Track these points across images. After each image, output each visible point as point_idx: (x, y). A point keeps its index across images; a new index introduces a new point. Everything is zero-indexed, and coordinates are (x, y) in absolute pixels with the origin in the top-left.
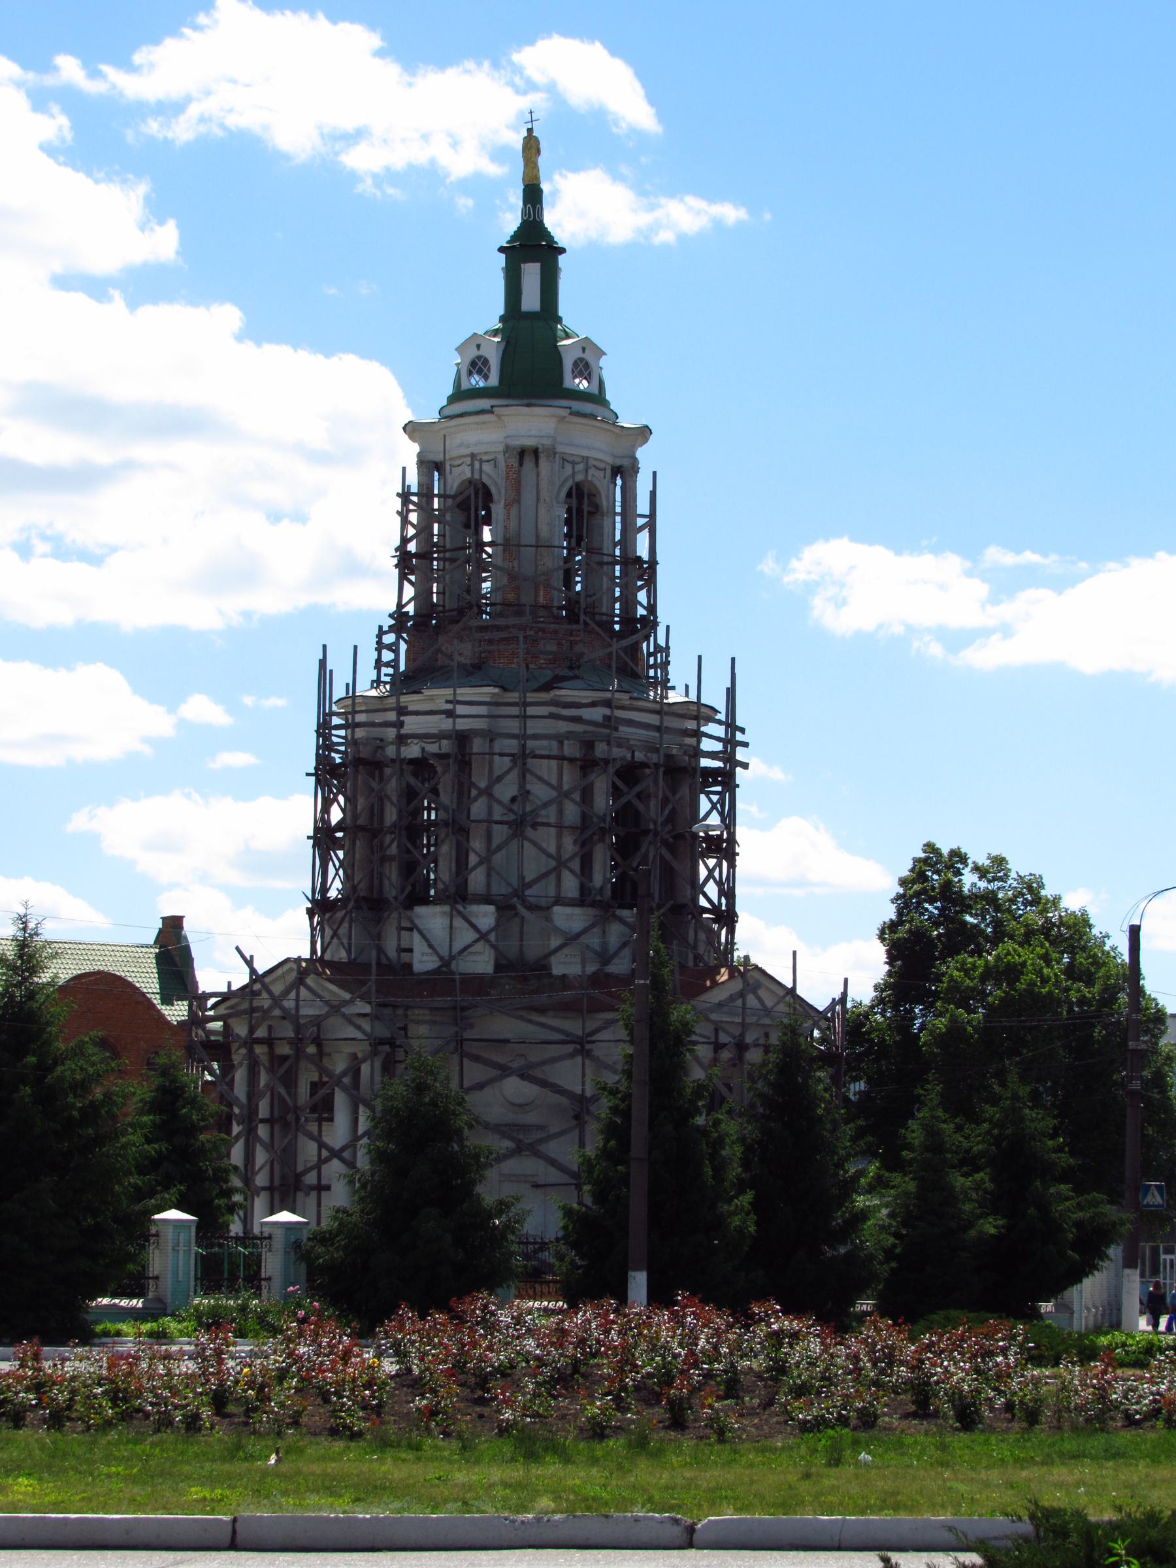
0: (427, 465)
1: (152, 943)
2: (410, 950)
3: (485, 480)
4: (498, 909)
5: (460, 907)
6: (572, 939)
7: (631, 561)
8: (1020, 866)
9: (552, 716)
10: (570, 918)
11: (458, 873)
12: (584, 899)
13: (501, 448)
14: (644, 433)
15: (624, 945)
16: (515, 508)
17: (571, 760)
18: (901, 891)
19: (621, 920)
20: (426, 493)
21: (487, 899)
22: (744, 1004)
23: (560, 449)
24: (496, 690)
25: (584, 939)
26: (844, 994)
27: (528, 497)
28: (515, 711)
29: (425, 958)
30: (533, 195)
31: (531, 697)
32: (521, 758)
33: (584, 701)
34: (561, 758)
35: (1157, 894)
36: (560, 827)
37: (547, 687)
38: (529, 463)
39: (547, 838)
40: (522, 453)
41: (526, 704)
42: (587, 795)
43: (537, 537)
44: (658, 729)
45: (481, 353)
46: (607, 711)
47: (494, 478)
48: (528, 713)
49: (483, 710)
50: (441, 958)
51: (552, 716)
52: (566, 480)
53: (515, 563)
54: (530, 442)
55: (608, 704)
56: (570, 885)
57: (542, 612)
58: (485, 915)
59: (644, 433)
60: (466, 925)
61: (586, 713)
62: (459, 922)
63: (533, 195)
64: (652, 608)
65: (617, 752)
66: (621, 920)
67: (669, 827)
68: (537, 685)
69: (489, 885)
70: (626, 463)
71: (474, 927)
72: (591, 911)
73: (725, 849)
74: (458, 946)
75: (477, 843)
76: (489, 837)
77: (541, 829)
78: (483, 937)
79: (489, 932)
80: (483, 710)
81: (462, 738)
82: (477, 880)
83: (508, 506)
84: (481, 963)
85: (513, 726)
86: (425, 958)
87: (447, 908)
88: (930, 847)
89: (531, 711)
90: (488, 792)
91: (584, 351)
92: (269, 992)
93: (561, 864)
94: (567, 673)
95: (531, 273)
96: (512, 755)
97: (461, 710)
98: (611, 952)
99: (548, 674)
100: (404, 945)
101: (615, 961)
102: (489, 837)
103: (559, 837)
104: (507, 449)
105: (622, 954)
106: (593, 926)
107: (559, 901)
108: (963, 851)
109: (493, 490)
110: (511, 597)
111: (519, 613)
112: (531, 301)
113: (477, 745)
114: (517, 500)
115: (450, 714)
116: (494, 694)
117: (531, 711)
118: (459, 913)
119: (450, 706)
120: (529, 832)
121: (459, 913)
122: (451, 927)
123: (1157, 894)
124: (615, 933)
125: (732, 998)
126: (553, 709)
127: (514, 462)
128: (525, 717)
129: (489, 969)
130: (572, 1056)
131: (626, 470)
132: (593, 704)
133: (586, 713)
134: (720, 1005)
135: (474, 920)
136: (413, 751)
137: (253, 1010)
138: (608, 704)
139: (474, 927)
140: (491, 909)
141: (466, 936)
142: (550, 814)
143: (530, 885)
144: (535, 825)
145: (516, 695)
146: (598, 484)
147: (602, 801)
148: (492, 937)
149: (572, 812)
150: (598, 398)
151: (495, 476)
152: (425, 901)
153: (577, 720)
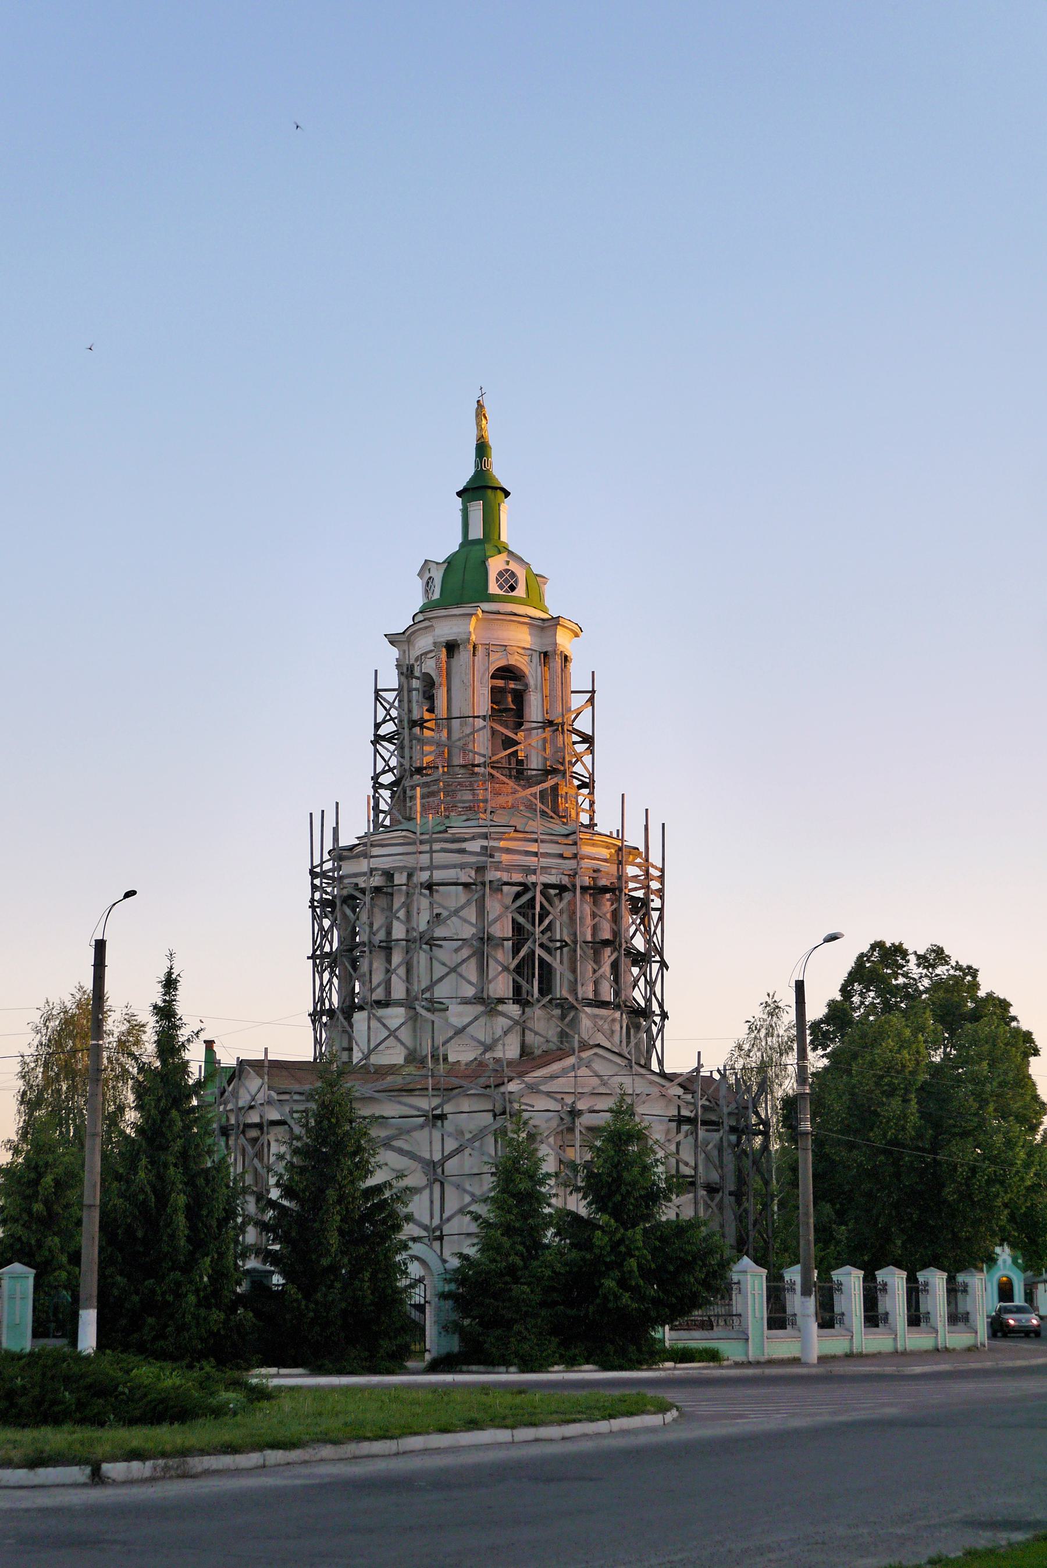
8: (959, 954)
18: (981, 994)
26: (700, 1066)
30: (482, 449)
35: (114, 904)
46: (485, 843)
53: (445, 733)
60: (380, 1025)
63: (482, 449)
67: (549, 934)
88: (901, 944)
91: (508, 564)
95: (477, 509)
97: (376, 851)
108: (905, 946)
112: (477, 532)
123: (114, 904)
129: (400, 1060)
130: (422, 1127)
146: (523, 667)
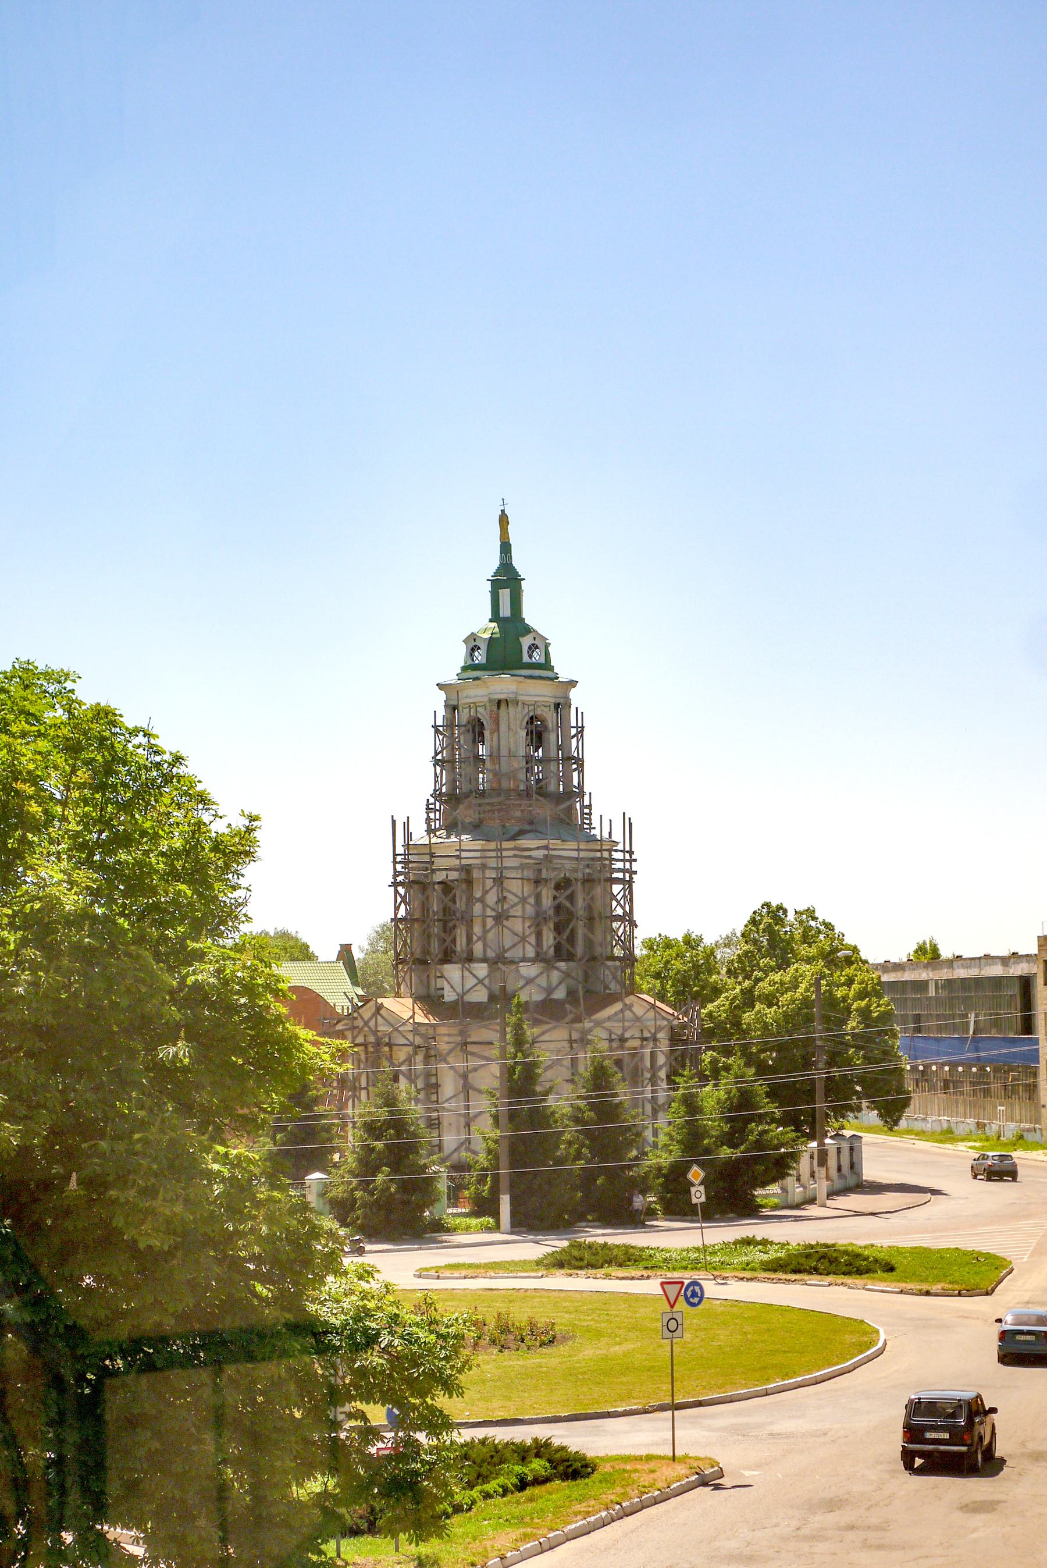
0: (452, 708)
1: (335, 960)
2: (443, 989)
3: (479, 716)
4: (490, 966)
5: (467, 966)
6: (529, 981)
7: (568, 759)
9: (515, 856)
10: (529, 970)
11: (468, 945)
12: (539, 957)
13: (486, 699)
14: (573, 683)
15: (560, 983)
16: (496, 734)
17: (528, 880)
19: (557, 969)
20: (450, 724)
21: (484, 960)
22: (623, 1016)
23: (521, 698)
24: (484, 842)
25: (538, 981)
27: (503, 727)
28: (494, 854)
29: (450, 994)
30: (506, 548)
31: (506, 845)
32: (499, 881)
33: (532, 847)
34: (522, 879)
36: (523, 918)
37: (513, 838)
38: (503, 707)
39: (518, 925)
40: (499, 702)
41: (501, 850)
42: (538, 897)
43: (510, 751)
44: (577, 859)
45: (476, 643)
46: (546, 852)
47: (484, 715)
48: (504, 855)
49: (478, 854)
50: (458, 995)
51: (515, 856)
52: (525, 716)
53: (497, 767)
54: (502, 697)
55: (546, 847)
56: (531, 952)
57: (513, 793)
58: (482, 968)
59: (573, 683)
61: (534, 854)
62: (466, 973)
63: (506, 548)
64: (581, 786)
65: (552, 875)
66: (557, 969)
68: (508, 836)
69: (485, 951)
70: (562, 701)
71: (475, 976)
72: (542, 965)
73: (628, 919)
74: (468, 986)
75: (477, 929)
76: (484, 925)
77: (511, 919)
78: (481, 982)
79: (484, 979)
80: (478, 854)
81: (467, 870)
82: (478, 948)
83: (492, 733)
84: (480, 996)
85: (493, 863)
86: (450, 994)
87: (460, 966)
89: (505, 854)
90: (482, 900)
92: (362, 1018)
93: (523, 939)
94: (527, 827)
95: (505, 594)
96: (494, 879)
97: (464, 854)
98: (554, 986)
99: (516, 829)
100: (438, 986)
101: (556, 991)
102: (484, 925)
103: (523, 922)
104: (490, 701)
105: (560, 987)
106: (541, 973)
107: (524, 959)
109: (485, 723)
110: (495, 785)
111: (499, 794)
112: (505, 611)
113: (476, 874)
114: (498, 730)
115: (458, 857)
116: (482, 845)
117: (505, 854)
118: (467, 968)
119: (458, 853)
120: (505, 923)
121: (467, 968)
122: (463, 977)
124: (555, 976)
125: (616, 1014)
126: (516, 852)
127: (495, 708)
128: (502, 857)
129: (485, 1000)
131: (561, 706)
132: (538, 848)
133: (534, 854)
134: (609, 1018)
135: (475, 972)
136: (439, 877)
137: (355, 1028)
138: (546, 847)
139: (475, 976)
140: (485, 965)
141: (471, 982)
142: (518, 911)
143: (506, 951)
144: (507, 918)
145: (494, 843)
146: (545, 715)
147: (547, 902)
148: (486, 982)
149: (530, 910)
150: (547, 665)
151: (485, 714)
152: (449, 961)
153: (529, 857)
